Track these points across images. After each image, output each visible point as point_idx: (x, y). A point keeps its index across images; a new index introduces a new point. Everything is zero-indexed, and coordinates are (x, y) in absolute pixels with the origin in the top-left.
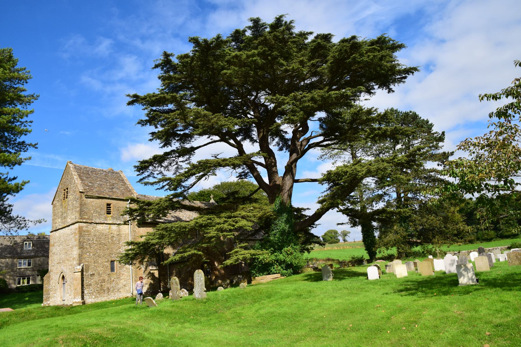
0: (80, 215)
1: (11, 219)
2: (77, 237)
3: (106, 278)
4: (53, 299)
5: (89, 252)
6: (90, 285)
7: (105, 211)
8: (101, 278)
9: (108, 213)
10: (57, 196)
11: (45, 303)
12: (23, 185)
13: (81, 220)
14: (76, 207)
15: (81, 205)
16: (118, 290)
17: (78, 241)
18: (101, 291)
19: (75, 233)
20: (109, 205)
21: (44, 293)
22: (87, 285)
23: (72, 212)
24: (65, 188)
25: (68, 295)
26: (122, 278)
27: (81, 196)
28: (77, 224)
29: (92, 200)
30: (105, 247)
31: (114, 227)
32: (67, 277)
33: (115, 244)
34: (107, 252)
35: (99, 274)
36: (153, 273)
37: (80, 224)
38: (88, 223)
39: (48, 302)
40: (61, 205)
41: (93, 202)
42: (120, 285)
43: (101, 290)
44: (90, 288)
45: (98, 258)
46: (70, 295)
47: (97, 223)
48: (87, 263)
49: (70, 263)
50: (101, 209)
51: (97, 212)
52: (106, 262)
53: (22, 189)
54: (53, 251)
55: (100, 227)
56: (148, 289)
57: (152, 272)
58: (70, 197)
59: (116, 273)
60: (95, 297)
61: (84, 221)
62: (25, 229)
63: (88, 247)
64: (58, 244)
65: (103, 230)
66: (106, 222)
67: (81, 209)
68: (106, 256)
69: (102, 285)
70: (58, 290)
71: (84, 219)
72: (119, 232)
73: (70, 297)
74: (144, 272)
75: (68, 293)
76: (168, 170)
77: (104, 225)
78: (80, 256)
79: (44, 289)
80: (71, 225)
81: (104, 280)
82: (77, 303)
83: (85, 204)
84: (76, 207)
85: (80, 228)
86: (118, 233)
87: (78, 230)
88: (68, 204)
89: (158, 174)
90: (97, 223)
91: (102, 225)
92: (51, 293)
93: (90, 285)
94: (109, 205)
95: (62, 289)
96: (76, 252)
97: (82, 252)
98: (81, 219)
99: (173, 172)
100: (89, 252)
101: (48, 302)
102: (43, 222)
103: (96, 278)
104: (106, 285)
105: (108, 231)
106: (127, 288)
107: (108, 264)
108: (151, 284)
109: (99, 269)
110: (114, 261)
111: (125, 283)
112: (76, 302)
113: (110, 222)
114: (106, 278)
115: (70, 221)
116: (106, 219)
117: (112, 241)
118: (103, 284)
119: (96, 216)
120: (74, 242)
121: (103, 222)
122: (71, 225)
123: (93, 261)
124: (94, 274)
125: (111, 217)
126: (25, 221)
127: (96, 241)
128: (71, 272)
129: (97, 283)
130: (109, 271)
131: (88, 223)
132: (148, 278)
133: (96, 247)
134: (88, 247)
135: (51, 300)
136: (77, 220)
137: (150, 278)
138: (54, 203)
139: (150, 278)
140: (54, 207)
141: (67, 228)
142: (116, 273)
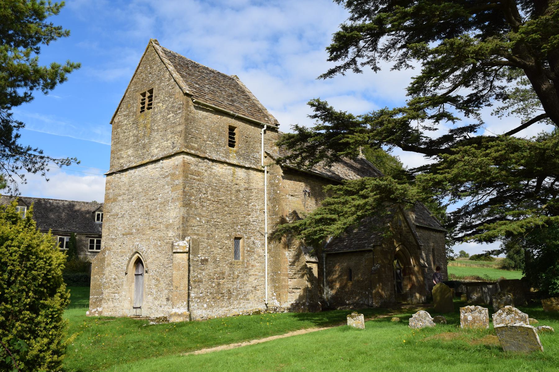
0: (186, 138)
1: (17, 151)
2: (180, 181)
3: (227, 270)
4: (110, 304)
5: (200, 215)
6: (200, 281)
7: (225, 139)
8: (218, 269)
9: (232, 144)
10: (124, 106)
11: (92, 312)
12: (68, 71)
13: (188, 151)
14: (174, 125)
15: (187, 119)
16: (245, 296)
17: (180, 191)
18: (220, 294)
19: (173, 175)
20: (232, 129)
21: (92, 290)
22: (195, 282)
23: (165, 135)
24: (146, 89)
25: (150, 298)
26: (251, 272)
27: (188, 102)
28: (180, 158)
29: (205, 113)
30: (226, 209)
31: (241, 173)
32: (148, 262)
33: (241, 205)
34: (229, 219)
35: (215, 261)
36: (310, 269)
37: (186, 157)
38: (198, 157)
39: (100, 309)
40: (136, 122)
41: (206, 118)
42: (248, 288)
43: (218, 292)
44: (199, 288)
45: (213, 229)
46: (155, 299)
47: (213, 161)
48: (195, 237)
49: (157, 234)
50: (220, 134)
51: (213, 139)
52: (227, 238)
53: (62, 80)
54: (114, 211)
55: (218, 169)
56: (301, 297)
57: (309, 265)
58: (159, 105)
59: (243, 262)
60: (209, 306)
61: (193, 152)
62: (39, 173)
63: (198, 204)
64: (125, 197)
65: (222, 175)
66: (228, 161)
67: (186, 129)
68: (226, 227)
69: (219, 284)
70: (125, 287)
71: (192, 148)
72: (248, 183)
73: (157, 303)
74: (293, 264)
75: (151, 294)
76: (386, 58)
77: (225, 167)
78: (185, 220)
79: (92, 283)
80: (162, 159)
81: (223, 274)
82: (180, 315)
83: (194, 120)
84: (174, 125)
85: (186, 164)
86: (246, 186)
87: (180, 169)
88: (154, 121)
89: (363, 64)
90: (213, 161)
91: (221, 166)
92: (106, 292)
93: (200, 281)
94: (232, 129)
95: (133, 285)
96: (174, 213)
97: (188, 214)
98: (187, 147)
99: (395, 63)
100: (200, 215)
101: (100, 309)
102: (73, 164)
103: (210, 268)
104: (227, 285)
105: (230, 178)
106: (259, 293)
107: (230, 243)
108: (306, 289)
109: (215, 252)
110: (240, 238)
111: (255, 283)
112: (176, 314)
113: (235, 162)
114: (227, 270)
115: (156, 152)
116: (227, 154)
117: (237, 198)
118: (221, 281)
119: (212, 146)
120: (170, 193)
121: (223, 160)
122: (162, 159)
123: (205, 234)
124: (207, 260)
125: (236, 152)
126: (42, 158)
127: (212, 194)
128: (159, 252)
129: (211, 279)
130: (231, 258)
131: (198, 157)
132: (302, 276)
133: (211, 208)
134: (198, 204)
135: (105, 305)
136: (176, 150)
137: (306, 277)
138: (116, 120)
139: (306, 277)
140: (115, 128)
141: (150, 166)
142: (243, 262)
